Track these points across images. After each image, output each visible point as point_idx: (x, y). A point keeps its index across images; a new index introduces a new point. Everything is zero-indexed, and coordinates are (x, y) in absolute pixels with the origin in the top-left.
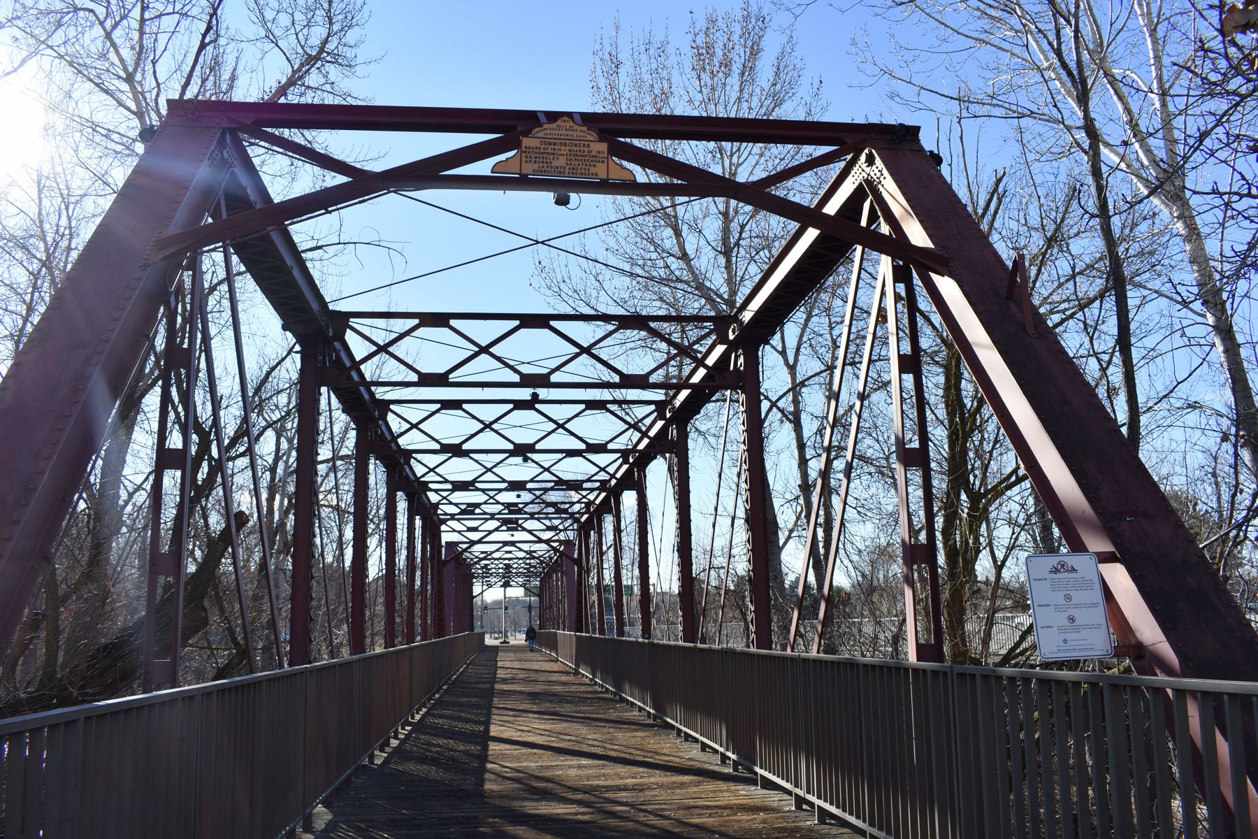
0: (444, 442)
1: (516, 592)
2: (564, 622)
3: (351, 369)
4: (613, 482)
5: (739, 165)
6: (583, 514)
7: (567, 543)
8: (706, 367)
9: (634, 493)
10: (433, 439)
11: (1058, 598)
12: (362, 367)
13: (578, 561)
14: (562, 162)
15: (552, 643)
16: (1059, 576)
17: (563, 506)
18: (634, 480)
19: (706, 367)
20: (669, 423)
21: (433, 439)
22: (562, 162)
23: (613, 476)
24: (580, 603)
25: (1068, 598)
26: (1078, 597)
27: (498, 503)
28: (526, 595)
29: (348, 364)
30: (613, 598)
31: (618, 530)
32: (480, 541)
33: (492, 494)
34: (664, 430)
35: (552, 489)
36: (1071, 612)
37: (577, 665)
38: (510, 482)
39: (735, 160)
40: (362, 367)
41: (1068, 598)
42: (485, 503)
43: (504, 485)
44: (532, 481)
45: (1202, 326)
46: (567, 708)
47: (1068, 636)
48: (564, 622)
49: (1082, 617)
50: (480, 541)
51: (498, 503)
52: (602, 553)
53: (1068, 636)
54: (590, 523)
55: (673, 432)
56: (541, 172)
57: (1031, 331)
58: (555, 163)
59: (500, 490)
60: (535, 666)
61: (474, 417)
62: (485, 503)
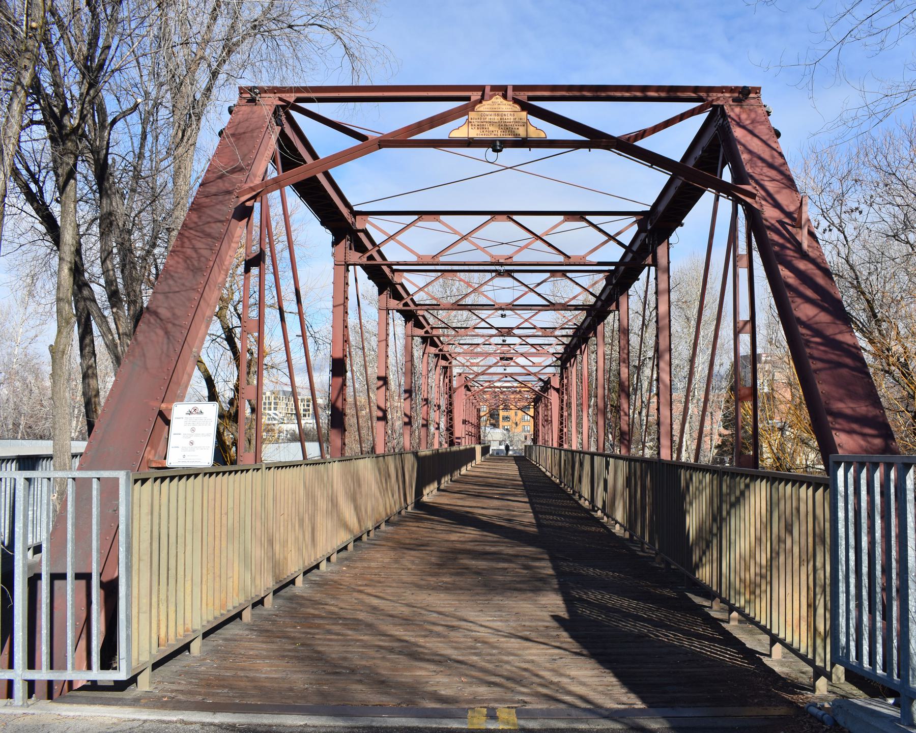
0: (584, 224)
3: (632, 252)
10: (595, 226)
11: (187, 430)
12: (627, 244)
16: (191, 416)
21: (595, 226)
25: (193, 430)
26: (199, 429)
29: (630, 255)
32: (483, 373)
36: (192, 438)
40: (627, 244)
41: (193, 430)
45: (661, 419)
47: (186, 453)
49: (198, 441)
50: (483, 373)
53: (186, 453)
61: (539, 295)
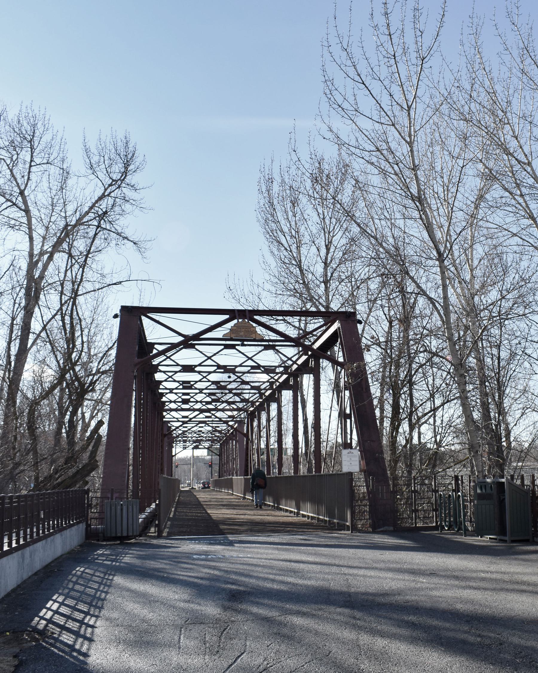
1: (202, 453)
2: (237, 473)
4: (295, 367)
5: (333, 236)
6: (267, 390)
7: (241, 423)
8: (297, 364)
9: (276, 404)
13: (246, 435)
14: (242, 334)
15: (229, 485)
17: (222, 384)
18: (275, 397)
19: (297, 364)
20: (310, 357)
22: (242, 334)
23: (295, 362)
24: (247, 460)
27: (175, 381)
28: (208, 455)
30: (264, 457)
31: (268, 420)
33: (170, 374)
34: (307, 361)
35: (214, 372)
37: (245, 494)
38: (183, 366)
39: (331, 234)
42: (166, 381)
43: (179, 368)
44: (200, 365)
46: (241, 508)
48: (237, 473)
51: (175, 381)
52: (260, 431)
54: (252, 416)
55: (312, 363)
56: (237, 337)
57: (364, 390)
58: (241, 334)
59: (176, 372)
60: (219, 497)
62: (166, 381)
